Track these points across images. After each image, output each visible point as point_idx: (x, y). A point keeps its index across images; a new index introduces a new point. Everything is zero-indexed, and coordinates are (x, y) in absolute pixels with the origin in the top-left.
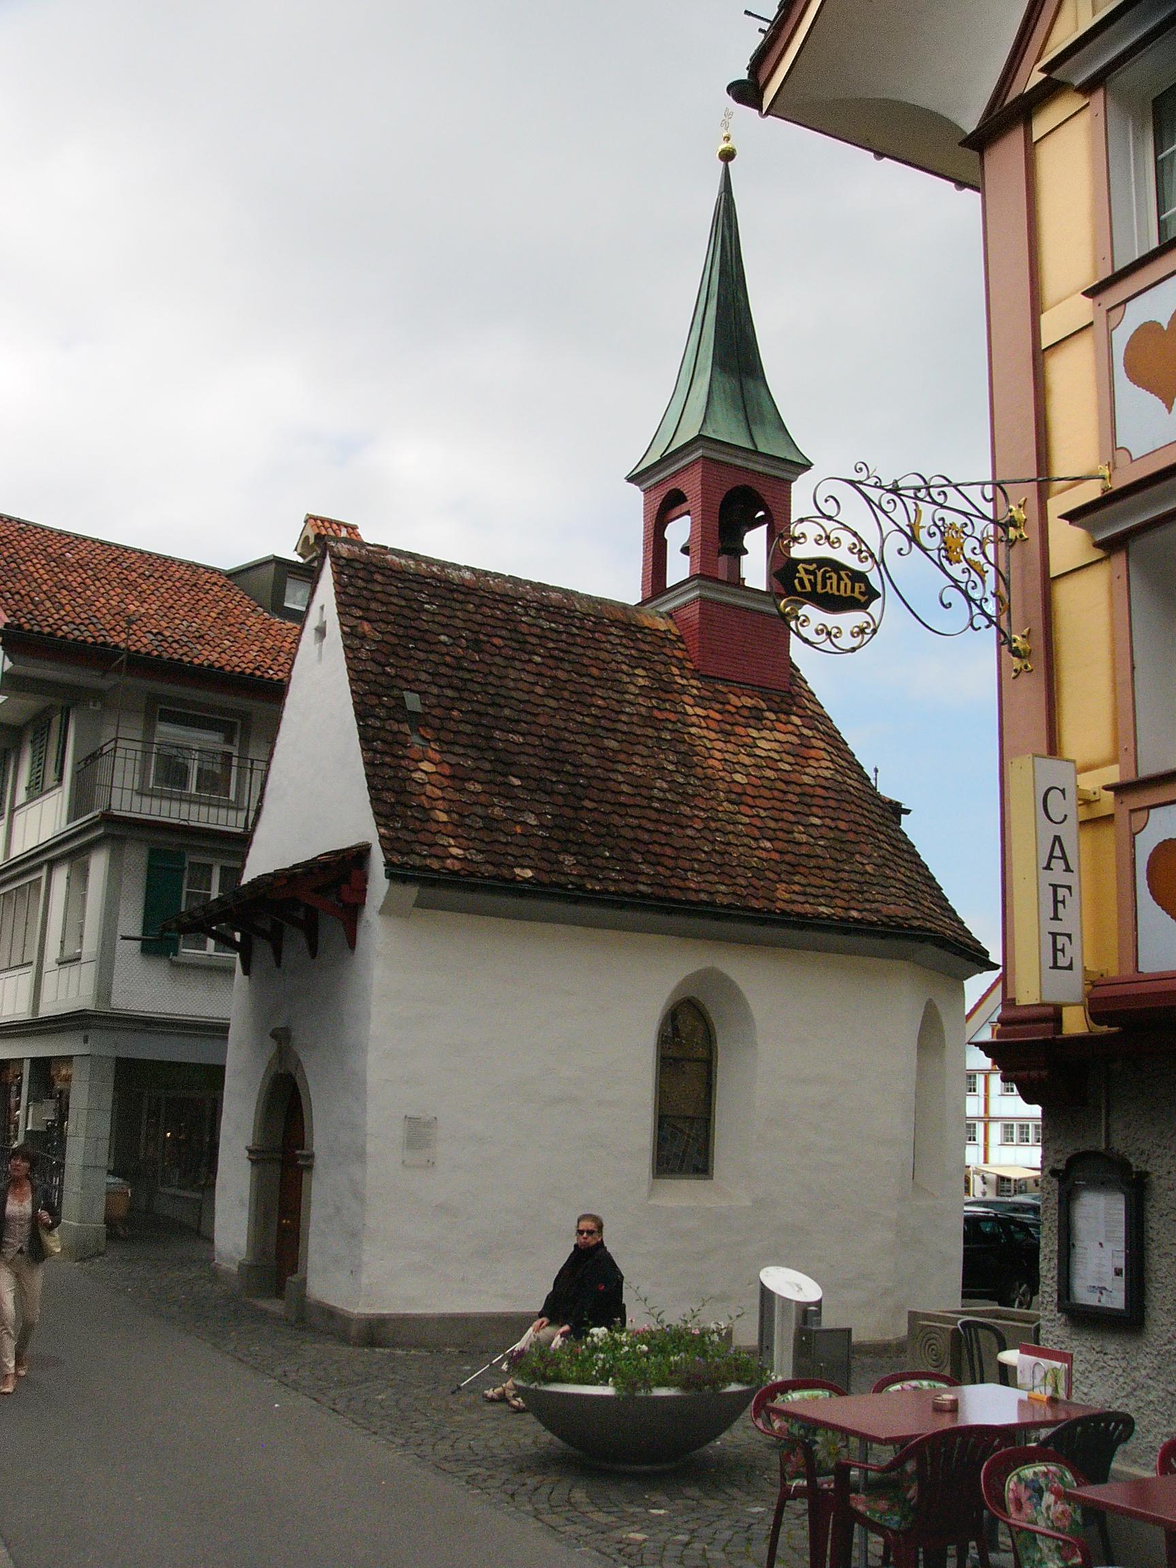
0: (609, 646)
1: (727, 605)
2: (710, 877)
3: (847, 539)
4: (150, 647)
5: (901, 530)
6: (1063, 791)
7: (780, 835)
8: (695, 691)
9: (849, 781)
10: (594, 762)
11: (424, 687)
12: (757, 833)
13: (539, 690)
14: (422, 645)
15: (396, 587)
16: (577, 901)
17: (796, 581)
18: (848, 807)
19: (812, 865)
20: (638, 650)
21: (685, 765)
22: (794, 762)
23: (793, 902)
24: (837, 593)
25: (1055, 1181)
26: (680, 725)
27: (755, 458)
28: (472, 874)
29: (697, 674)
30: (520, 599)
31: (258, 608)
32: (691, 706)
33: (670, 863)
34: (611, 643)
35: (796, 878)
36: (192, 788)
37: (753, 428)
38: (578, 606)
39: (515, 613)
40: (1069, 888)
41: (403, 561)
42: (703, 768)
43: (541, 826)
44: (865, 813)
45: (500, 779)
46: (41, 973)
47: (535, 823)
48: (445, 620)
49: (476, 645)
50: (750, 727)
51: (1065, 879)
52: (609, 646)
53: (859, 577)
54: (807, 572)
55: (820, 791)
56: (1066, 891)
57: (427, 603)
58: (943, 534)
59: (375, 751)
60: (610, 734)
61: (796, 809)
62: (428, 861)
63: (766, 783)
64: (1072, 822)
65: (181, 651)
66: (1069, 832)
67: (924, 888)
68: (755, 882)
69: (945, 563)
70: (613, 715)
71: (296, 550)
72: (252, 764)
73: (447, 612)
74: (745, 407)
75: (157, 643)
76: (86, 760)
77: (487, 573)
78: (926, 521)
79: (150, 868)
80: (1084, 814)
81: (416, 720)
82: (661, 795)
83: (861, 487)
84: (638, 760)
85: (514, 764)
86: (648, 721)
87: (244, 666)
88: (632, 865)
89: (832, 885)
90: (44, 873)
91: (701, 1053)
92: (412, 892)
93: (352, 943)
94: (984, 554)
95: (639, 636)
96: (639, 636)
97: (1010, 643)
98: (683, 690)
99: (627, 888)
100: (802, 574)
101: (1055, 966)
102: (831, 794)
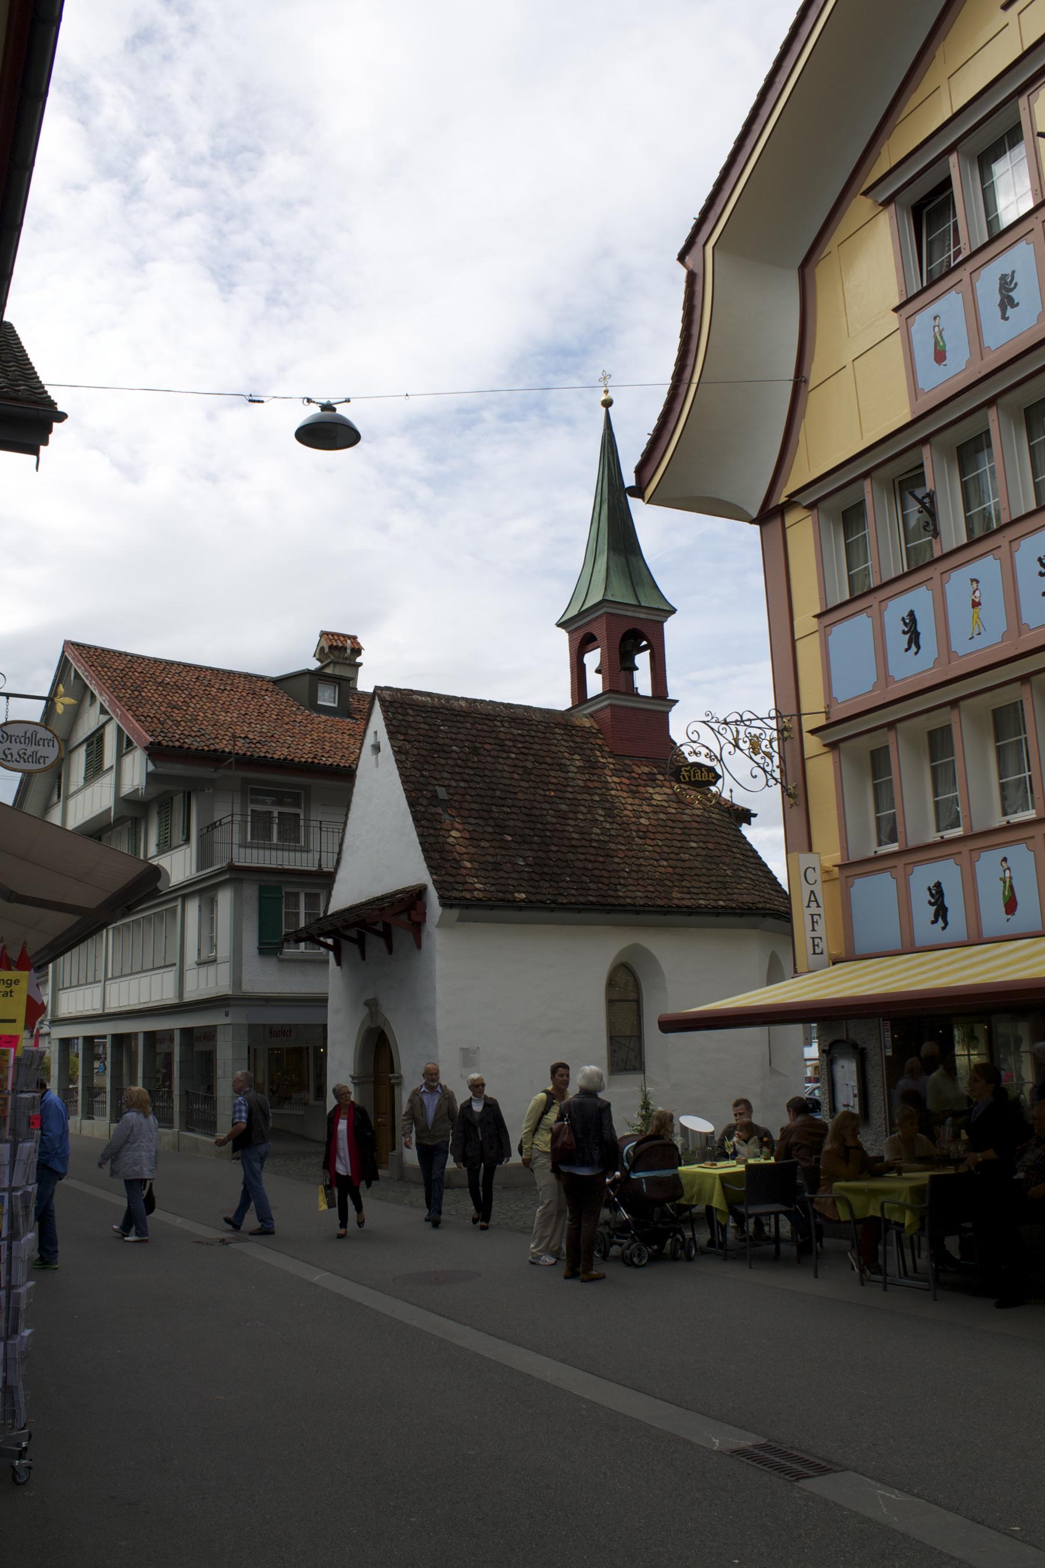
0: (556, 742)
1: (627, 708)
2: (631, 888)
3: (704, 751)
4: (245, 749)
5: (730, 743)
6: (814, 869)
7: (672, 856)
8: (612, 766)
9: (714, 816)
10: (554, 820)
11: (446, 783)
12: (658, 857)
13: (516, 776)
14: (442, 755)
15: (422, 716)
16: (553, 910)
17: (681, 776)
18: (713, 834)
19: (693, 874)
20: (574, 742)
21: (610, 816)
22: (677, 807)
23: (683, 899)
24: (700, 779)
25: (825, 1055)
26: (604, 790)
27: (638, 609)
28: (490, 900)
29: (612, 754)
30: (497, 716)
31: (300, 707)
32: (610, 776)
33: (605, 881)
34: (557, 740)
35: (684, 884)
36: (275, 840)
37: (638, 590)
38: (534, 717)
39: (496, 726)
40: (819, 915)
41: (423, 698)
42: (621, 817)
43: (528, 865)
44: (725, 835)
45: (498, 837)
46: (183, 972)
47: (522, 863)
48: (454, 736)
49: (475, 751)
50: (649, 786)
51: (820, 911)
52: (556, 742)
53: (712, 769)
54: (686, 771)
55: (695, 825)
56: (818, 917)
57: (442, 726)
58: (750, 740)
59: (423, 827)
60: (562, 801)
61: (680, 838)
62: (464, 894)
63: (661, 823)
64: (819, 882)
65: (264, 750)
66: (818, 889)
67: (765, 880)
68: (659, 888)
69: (753, 755)
70: (563, 789)
71: (314, 656)
72: (321, 824)
73: (454, 730)
74: (631, 577)
75: (247, 746)
76: (208, 827)
77: (475, 701)
78: (742, 735)
79: (261, 898)
80: (826, 878)
81: (446, 804)
82: (596, 837)
83: (709, 723)
84: (581, 816)
85: (506, 826)
86: (587, 790)
87: (306, 756)
88: (584, 884)
89: (707, 886)
90: (179, 903)
91: (633, 996)
92: (455, 913)
93: (419, 947)
94: (771, 747)
95: (573, 732)
96: (573, 732)
97: (787, 791)
98: (604, 766)
99: (582, 899)
100: (684, 773)
101: (814, 953)
102: (702, 826)
